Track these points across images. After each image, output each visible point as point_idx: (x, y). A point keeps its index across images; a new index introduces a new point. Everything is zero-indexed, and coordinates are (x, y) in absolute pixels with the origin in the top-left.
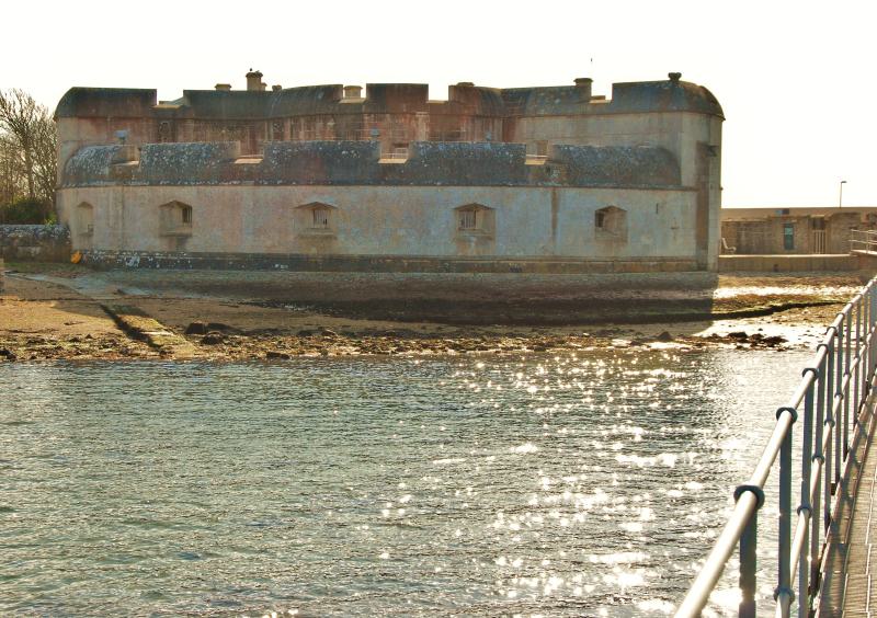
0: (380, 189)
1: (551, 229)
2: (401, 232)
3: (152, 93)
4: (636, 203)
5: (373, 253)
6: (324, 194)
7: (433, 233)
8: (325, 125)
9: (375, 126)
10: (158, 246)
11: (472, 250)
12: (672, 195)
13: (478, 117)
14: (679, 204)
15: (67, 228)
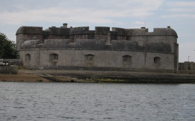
0: (105, 51)
1: (144, 62)
2: (110, 61)
3: (88, 28)
4: (163, 57)
5: (104, 66)
6: (92, 52)
7: (118, 62)
8: (85, 36)
9: (98, 37)
10: (49, 64)
11: (127, 66)
12: (170, 55)
13: (122, 35)
14: (171, 57)
15: (22, 60)
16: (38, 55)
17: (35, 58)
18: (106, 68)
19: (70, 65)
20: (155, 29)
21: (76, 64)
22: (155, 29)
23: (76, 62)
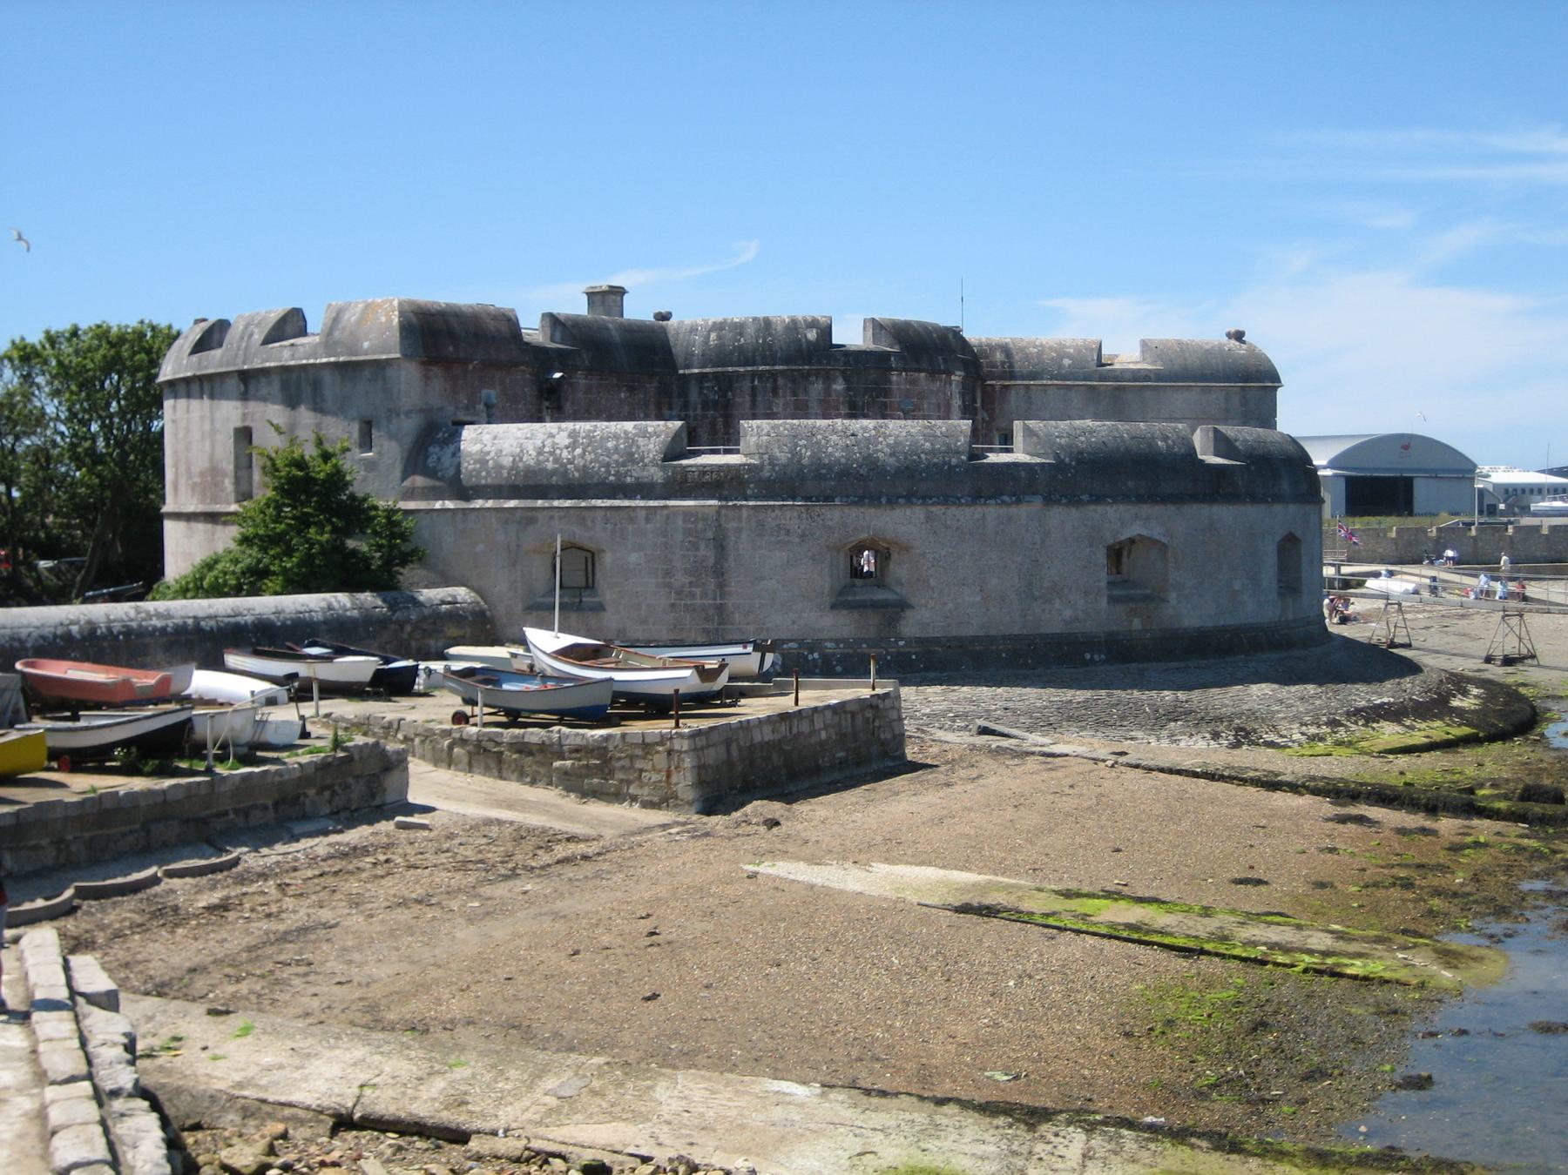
8: (828, 391)
16: (707, 553)
17: (668, 573)
18: (1237, 631)
19: (1016, 630)
20: (878, 327)
21: (1056, 618)
22: (878, 327)
23: (1057, 604)
